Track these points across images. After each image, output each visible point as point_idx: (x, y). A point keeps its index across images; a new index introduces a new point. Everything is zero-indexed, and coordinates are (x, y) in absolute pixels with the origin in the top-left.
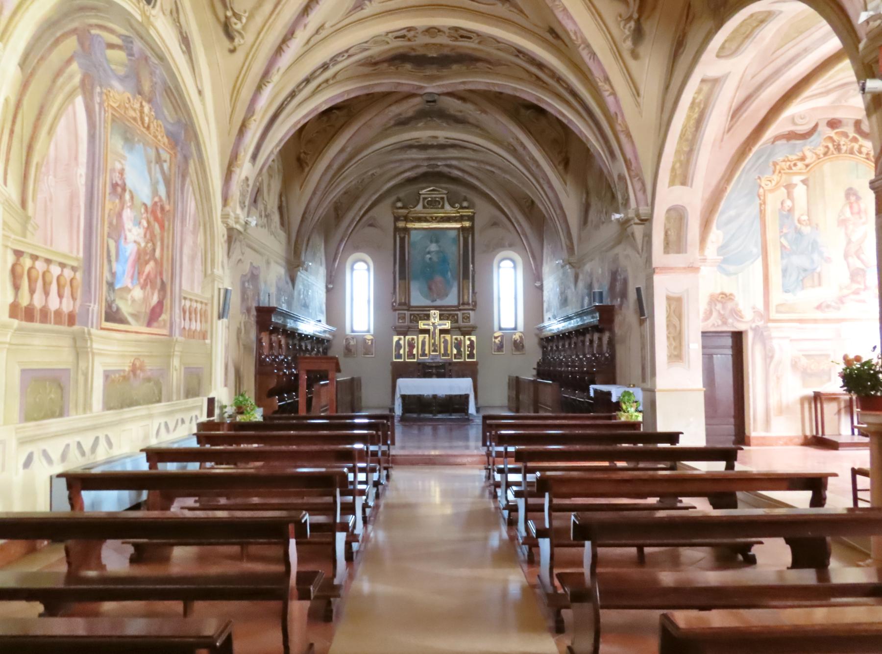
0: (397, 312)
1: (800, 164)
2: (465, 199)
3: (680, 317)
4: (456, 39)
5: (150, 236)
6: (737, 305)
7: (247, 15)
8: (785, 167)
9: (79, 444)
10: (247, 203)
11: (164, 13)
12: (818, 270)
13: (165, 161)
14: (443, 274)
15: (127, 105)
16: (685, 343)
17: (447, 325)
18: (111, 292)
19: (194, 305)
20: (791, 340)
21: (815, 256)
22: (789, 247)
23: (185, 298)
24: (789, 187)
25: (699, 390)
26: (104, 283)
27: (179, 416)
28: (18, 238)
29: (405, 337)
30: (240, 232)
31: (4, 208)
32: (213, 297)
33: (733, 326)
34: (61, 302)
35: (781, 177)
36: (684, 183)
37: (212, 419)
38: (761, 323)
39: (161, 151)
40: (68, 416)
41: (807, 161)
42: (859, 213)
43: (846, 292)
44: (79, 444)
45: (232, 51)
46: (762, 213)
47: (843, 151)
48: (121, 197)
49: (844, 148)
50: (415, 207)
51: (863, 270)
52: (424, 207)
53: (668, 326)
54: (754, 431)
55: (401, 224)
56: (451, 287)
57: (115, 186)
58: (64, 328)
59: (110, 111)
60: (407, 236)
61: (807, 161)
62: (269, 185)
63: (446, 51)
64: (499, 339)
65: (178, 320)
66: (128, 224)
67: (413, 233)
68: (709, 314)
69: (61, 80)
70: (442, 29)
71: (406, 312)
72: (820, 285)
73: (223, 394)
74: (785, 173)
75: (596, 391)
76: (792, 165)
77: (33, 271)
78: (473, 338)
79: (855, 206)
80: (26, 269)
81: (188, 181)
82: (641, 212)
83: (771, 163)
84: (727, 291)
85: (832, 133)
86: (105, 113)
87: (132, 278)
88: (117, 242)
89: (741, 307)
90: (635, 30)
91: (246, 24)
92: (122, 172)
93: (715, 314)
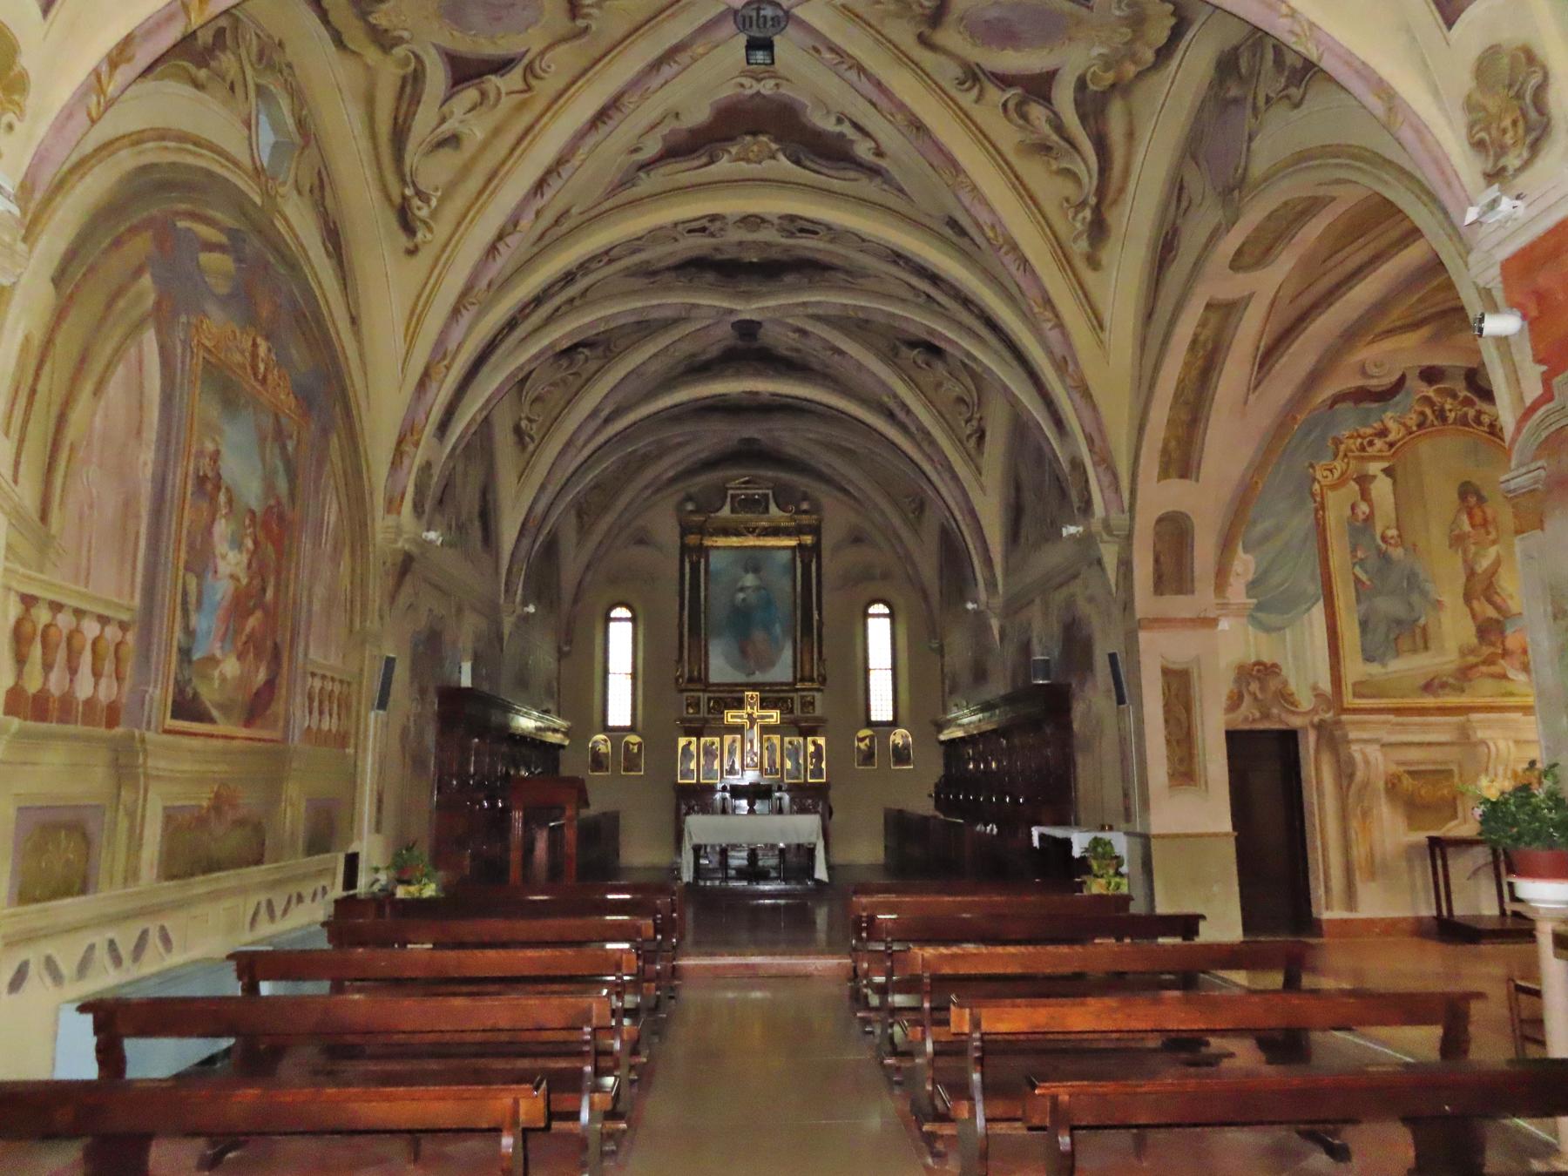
0: (686, 694)
1: (1379, 443)
2: (805, 497)
3: (1188, 709)
4: (791, 235)
5: (258, 567)
6: (1285, 683)
7: (439, 194)
8: (1353, 447)
9: (112, 943)
10: (427, 508)
11: (300, 193)
12: (1422, 621)
13: (291, 437)
14: (767, 628)
15: (230, 344)
16: (1198, 750)
17: (774, 716)
18: (186, 665)
19: (329, 686)
20: (1383, 745)
21: (1415, 598)
22: (1368, 583)
23: (313, 675)
24: (1364, 481)
25: (1227, 835)
26: (175, 649)
27: (293, 889)
28: (28, 572)
29: (698, 740)
30: (229, 396)
31: (11, 524)
32: (362, 670)
33: (1281, 721)
34: (96, 685)
35: (1348, 464)
36: (1184, 474)
37: (351, 892)
38: (1329, 716)
39: (284, 420)
40: (95, 892)
41: (1391, 437)
42: (1485, 523)
43: (1472, 659)
44: (112, 943)
45: (412, 252)
46: (1320, 528)
47: (1451, 420)
48: (213, 499)
49: (1452, 416)
50: (718, 510)
51: (1498, 621)
52: (733, 511)
53: (1166, 721)
54: (1327, 908)
55: (692, 539)
56: (781, 650)
57: (201, 480)
58: (101, 731)
59: (202, 353)
60: (703, 560)
61: (1391, 437)
62: (465, 474)
63: (775, 254)
64: (867, 741)
65: (298, 714)
66: (221, 547)
67: (713, 556)
68: (1235, 702)
69: (121, 304)
70: (768, 217)
71: (701, 694)
72: (1426, 648)
73: (371, 848)
74: (1355, 458)
75: (1042, 837)
76: (1365, 443)
77: (52, 630)
78: (821, 741)
79: (1478, 513)
80: (40, 627)
81: (328, 467)
82: (1112, 522)
83: (1330, 442)
84: (1266, 659)
85: (1430, 392)
86: (192, 358)
87: (223, 640)
88: (200, 576)
89: (1292, 687)
90: (1092, 223)
91: (436, 208)
92: (216, 457)
93: (1247, 699)
